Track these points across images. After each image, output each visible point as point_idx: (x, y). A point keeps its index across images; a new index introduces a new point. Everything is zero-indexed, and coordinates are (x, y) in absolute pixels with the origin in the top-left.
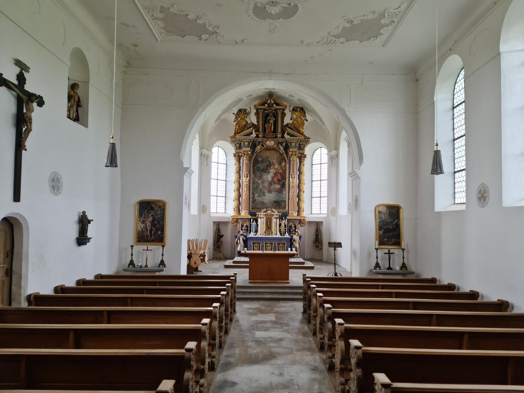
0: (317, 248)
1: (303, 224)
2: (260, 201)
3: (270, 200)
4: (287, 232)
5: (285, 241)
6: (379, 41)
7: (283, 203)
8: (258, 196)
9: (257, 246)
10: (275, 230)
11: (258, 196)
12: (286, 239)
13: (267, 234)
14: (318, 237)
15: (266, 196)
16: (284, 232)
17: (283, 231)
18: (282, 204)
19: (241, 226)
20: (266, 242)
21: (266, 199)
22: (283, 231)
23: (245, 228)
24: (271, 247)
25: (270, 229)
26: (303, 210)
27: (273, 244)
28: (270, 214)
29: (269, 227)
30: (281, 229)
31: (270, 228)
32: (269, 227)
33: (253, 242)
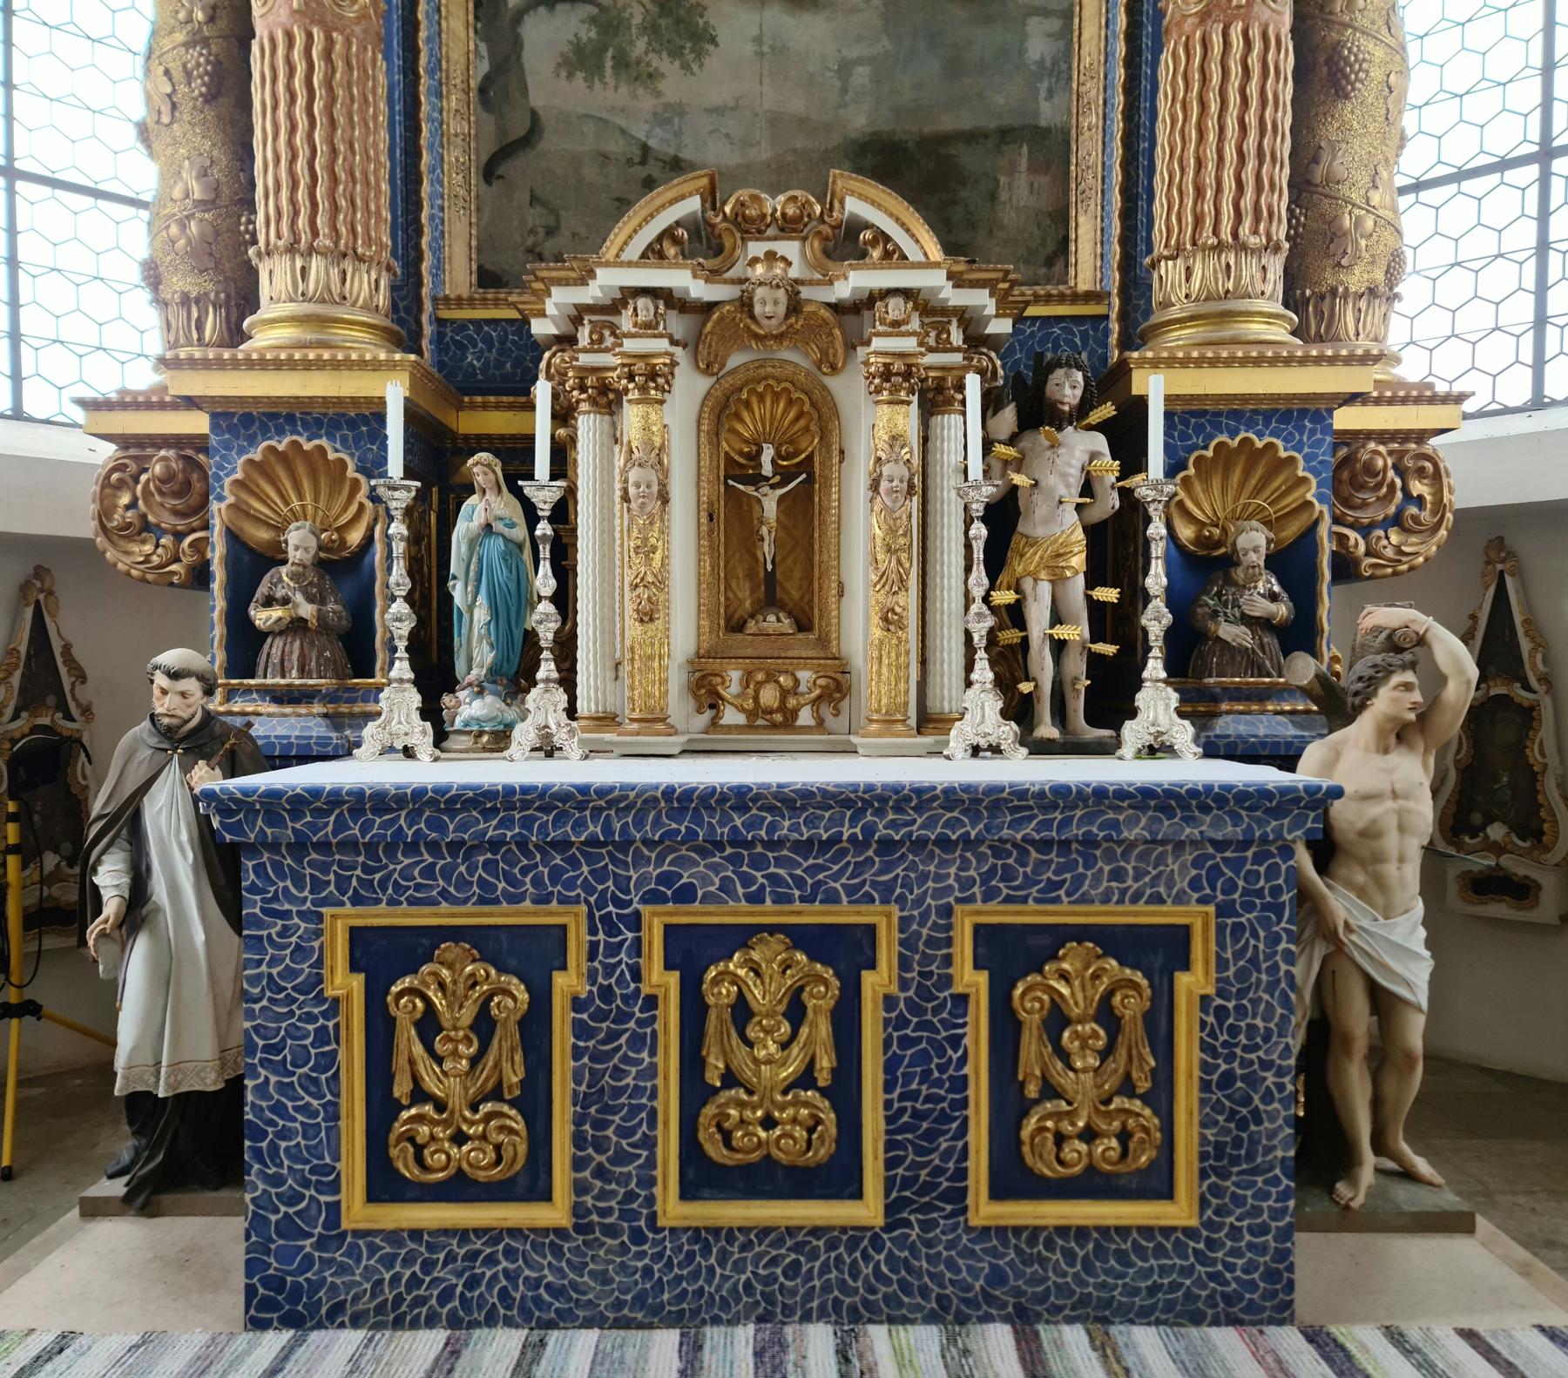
0: (1500, 909)
1: (1397, 521)
2: (615, 146)
3: (802, 123)
4: (1155, 668)
5: (1180, 869)
6: (978, 509)
7: (1022, 181)
8: (582, 60)
9: (484, 1025)
10: (890, 620)
11: (582, 60)
12: (1205, 826)
13: (731, 716)
14: (1519, 749)
15: (713, 61)
16: (1077, 666)
17: (1059, 647)
18: (993, 197)
19: (231, 563)
20: (685, 916)
21: (718, 111)
22: (1059, 647)
23: (307, 610)
24: (819, 1029)
25: (803, 625)
26: (1394, 267)
27: (886, 953)
28: (795, 306)
29: (770, 578)
30: (1015, 615)
31: (791, 590)
32: (770, 578)
33: (380, 916)
